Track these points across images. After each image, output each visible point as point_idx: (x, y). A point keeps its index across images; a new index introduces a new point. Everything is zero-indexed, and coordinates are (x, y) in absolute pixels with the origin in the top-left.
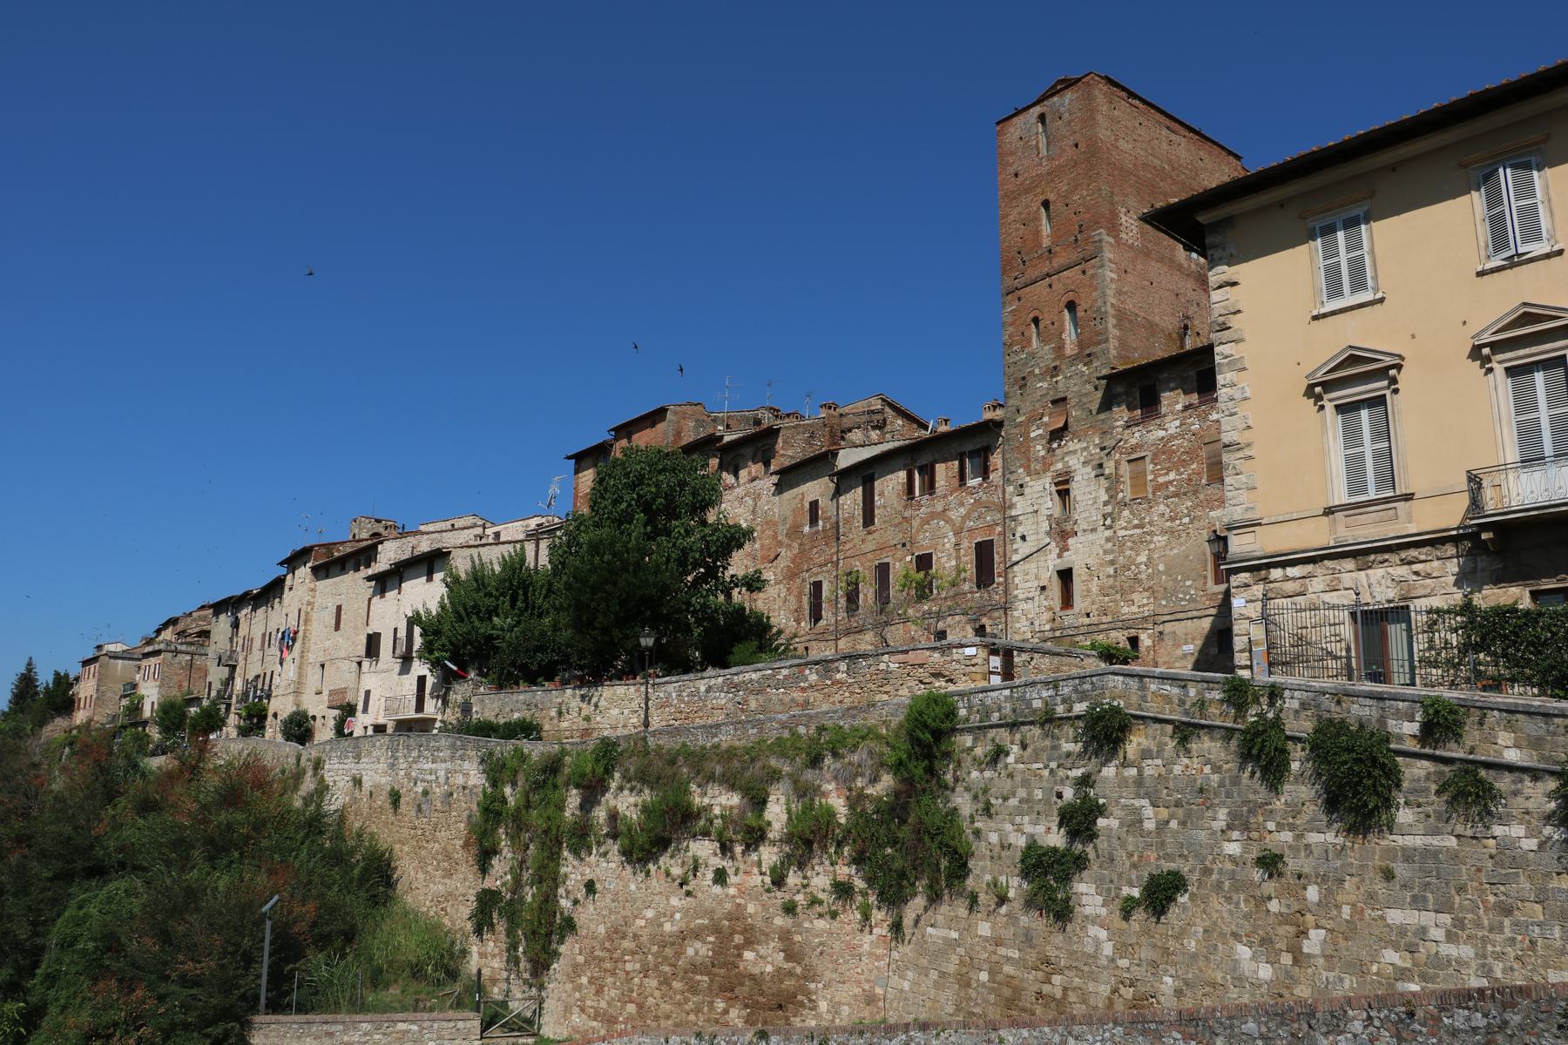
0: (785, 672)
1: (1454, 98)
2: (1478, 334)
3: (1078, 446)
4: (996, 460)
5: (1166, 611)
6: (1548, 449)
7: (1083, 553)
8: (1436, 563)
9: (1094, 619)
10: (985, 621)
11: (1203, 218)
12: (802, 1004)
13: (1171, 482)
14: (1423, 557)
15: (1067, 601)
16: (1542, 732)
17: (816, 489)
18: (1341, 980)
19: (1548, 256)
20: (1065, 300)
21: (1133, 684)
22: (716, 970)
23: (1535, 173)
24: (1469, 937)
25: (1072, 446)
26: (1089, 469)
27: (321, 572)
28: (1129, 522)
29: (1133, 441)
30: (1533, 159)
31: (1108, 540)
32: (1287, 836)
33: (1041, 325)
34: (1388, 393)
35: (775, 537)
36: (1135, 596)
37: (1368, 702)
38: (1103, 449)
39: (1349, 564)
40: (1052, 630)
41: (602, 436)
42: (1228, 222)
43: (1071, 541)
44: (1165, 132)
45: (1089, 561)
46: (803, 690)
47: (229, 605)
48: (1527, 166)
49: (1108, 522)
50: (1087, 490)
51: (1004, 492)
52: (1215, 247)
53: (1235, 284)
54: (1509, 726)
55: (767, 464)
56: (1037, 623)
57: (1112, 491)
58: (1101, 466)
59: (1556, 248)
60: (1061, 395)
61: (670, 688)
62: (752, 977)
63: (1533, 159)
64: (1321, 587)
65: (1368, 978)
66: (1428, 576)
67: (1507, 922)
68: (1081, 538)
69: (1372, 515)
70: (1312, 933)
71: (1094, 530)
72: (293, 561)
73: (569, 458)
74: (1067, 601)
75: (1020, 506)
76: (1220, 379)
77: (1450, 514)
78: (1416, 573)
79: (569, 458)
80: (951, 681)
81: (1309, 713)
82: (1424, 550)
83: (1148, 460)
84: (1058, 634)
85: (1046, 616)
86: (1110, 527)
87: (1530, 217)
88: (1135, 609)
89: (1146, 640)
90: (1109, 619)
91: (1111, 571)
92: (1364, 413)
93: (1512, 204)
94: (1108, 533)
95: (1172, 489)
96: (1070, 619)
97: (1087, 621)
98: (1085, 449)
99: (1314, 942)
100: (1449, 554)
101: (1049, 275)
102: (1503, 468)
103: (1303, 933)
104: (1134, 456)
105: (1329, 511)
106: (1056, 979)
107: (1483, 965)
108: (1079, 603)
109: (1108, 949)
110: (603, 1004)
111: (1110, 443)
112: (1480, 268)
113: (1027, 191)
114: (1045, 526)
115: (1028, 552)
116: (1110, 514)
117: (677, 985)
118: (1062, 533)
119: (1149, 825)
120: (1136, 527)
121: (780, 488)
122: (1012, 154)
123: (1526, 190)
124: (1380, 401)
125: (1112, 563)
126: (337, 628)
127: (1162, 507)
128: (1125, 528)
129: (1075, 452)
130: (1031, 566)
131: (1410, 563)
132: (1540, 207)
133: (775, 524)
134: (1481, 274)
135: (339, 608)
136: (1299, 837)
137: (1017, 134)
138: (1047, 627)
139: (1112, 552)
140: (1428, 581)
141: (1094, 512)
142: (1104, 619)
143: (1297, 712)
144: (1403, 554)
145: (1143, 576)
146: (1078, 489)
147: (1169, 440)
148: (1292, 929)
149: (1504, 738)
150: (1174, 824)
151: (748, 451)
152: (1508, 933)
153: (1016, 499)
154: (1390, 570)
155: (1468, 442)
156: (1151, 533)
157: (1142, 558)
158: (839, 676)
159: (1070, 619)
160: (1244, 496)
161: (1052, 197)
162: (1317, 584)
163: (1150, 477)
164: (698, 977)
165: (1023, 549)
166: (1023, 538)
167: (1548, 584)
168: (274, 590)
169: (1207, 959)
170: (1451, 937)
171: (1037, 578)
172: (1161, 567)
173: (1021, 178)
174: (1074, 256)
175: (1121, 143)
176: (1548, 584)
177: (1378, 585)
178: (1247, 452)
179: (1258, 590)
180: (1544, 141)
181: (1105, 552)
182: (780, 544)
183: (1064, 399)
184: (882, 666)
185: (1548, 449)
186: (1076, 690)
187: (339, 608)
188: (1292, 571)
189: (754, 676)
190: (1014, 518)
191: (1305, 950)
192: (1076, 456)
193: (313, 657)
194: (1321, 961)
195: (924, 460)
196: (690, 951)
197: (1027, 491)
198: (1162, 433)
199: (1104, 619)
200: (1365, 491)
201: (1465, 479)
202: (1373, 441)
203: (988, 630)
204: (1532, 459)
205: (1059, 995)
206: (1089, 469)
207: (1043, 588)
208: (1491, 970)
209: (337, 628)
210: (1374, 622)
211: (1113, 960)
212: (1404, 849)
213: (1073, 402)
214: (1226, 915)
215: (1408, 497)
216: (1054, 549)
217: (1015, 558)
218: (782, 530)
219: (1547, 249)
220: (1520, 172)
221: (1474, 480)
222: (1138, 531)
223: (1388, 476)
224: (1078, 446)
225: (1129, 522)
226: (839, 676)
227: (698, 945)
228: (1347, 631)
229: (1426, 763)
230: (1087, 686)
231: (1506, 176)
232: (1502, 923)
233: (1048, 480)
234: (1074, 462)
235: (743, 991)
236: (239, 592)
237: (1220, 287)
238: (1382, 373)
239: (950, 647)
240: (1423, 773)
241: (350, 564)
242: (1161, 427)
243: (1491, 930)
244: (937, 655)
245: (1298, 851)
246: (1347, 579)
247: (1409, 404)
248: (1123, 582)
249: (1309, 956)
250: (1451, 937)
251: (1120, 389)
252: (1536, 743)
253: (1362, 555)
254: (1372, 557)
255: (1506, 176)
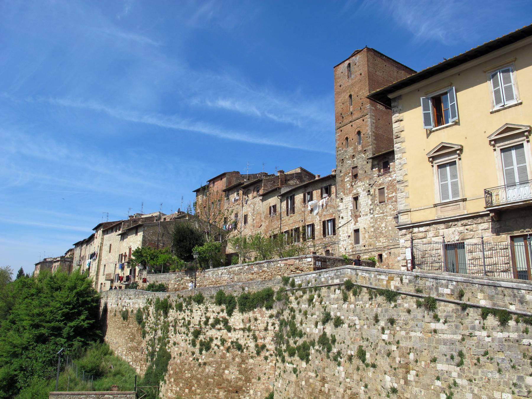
0: (247, 267)
1: (479, 46)
2: (490, 136)
3: (361, 184)
4: (333, 189)
5: (392, 244)
6: (517, 180)
7: (363, 223)
8: (474, 226)
9: (367, 248)
10: (329, 248)
11: (390, 96)
12: (244, 391)
13: (393, 197)
14: (469, 223)
15: (357, 241)
16: (493, 294)
17: (273, 200)
18: (421, 391)
19: (516, 105)
20: (357, 131)
21: (354, 272)
22: (215, 377)
23: (511, 73)
24: (466, 377)
25: (360, 184)
26: (365, 192)
27: (105, 232)
28: (379, 212)
29: (380, 182)
30: (510, 68)
31: (371, 218)
32: (403, 333)
33: (349, 140)
34: (457, 160)
35: (260, 219)
36: (381, 239)
37: (432, 280)
38: (370, 185)
39: (442, 226)
40: (353, 252)
41: (205, 184)
42: (399, 97)
43: (359, 219)
44: (395, 69)
45: (365, 226)
46: (252, 274)
47: (79, 244)
48: (508, 71)
49: (372, 212)
50: (364, 201)
51: (336, 201)
52: (394, 107)
53: (402, 120)
54: (482, 291)
55: (258, 191)
56: (347, 249)
57: (373, 200)
58: (369, 191)
59: (519, 102)
60: (355, 165)
61: (210, 273)
62: (227, 380)
63: (510, 68)
64: (431, 235)
65: (430, 391)
66: (471, 230)
67: (480, 371)
68: (362, 218)
69: (451, 207)
70: (411, 372)
71: (367, 215)
72: (97, 229)
73: (194, 191)
74: (357, 241)
75: (342, 206)
76: (396, 156)
77: (479, 206)
78: (467, 229)
79: (194, 191)
80: (302, 271)
81: (411, 284)
82: (470, 220)
83: (385, 188)
84: (354, 253)
85: (350, 247)
86: (372, 214)
87: (509, 90)
88: (381, 244)
89: (385, 256)
90: (372, 248)
91: (372, 230)
92: (448, 168)
93: (502, 86)
94: (372, 216)
95: (394, 199)
96: (359, 247)
97: (364, 248)
98: (364, 185)
99: (411, 377)
100: (479, 222)
101: (351, 122)
102: (497, 188)
103: (408, 372)
104: (381, 187)
105: (435, 206)
106: (326, 385)
107: (471, 388)
108: (361, 242)
109: (343, 375)
110: (178, 389)
111: (372, 183)
112: (491, 111)
113: (344, 91)
114: (350, 213)
115: (344, 223)
116: (372, 209)
117: (202, 382)
118: (356, 216)
119: (358, 327)
120: (381, 213)
121: (262, 200)
122: (339, 78)
123: (507, 80)
124: (454, 163)
125: (373, 227)
126: (110, 252)
127: (390, 206)
128: (377, 214)
129: (360, 186)
130: (345, 228)
131: (465, 225)
132: (513, 86)
133: (261, 214)
134: (491, 113)
135: (111, 245)
136: (407, 333)
137: (341, 71)
138: (351, 251)
139: (373, 223)
140: (472, 232)
141: (367, 208)
142: (370, 248)
143: (407, 284)
144: (462, 222)
145: (384, 232)
146: (361, 200)
147: (393, 181)
148: (404, 370)
149: (480, 296)
150: (365, 327)
151: (252, 188)
152: (480, 375)
153: (340, 204)
154: (457, 228)
155: (485, 177)
156: (387, 216)
157: (383, 225)
158: (264, 269)
159: (359, 247)
160: (403, 201)
161: (352, 93)
162: (430, 234)
163: (386, 195)
164: (210, 380)
165: (342, 222)
166: (342, 218)
167: (517, 233)
168: (92, 238)
169: (375, 380)
170: (459, 376)
171: (347, 232)
172: (390, 228)
173: (342, 87)
174: (360, 115)
175: (378, 73)
176: (517, 233)
177: (452, 234)
178: (406, 184)
179: (409, 236)
180: (515, 61)
181: (371, 223)
182: (262, 221)
183: (356, 167)
184: (279, 265)
185: (517, 180)
186: (335, 275)
187: (111, 245)
188: (421, 229)
189: (237, 269)
190: (339, 211)
191: (409, 379)
192: (361, 188)
193: (103, 263)
194: (414, 383)
195: (309, 190)
196: (207, 370)
197: (344, 201)
198: (390, 179)
199: (370, 248)
200: (448, 198)
201: (483, 193)
202: (451, 179)
203: (330, 252)
204: (511, 184)
205: (327, 392)
206: (365, 192)
207: (349, 236)
208: (473, 391)
209: (110, 252)
210: (454, 248)
211: (345, 379)
212: (444, 340)
213: (360, 168)
214: (382, 363)
215: (464, 200)
216: (353, 222)
217: (340, 225)
218: (263, 216)
219: (516, 103)
220: (505, 74)
221: (488, 193)
222: (382, 215)
223: (455, 193)
224: (361, 184)
225: (379, 212)
226: (264, 269)
227: (210, 367)
228: (441, 252)
229: (452, 305)
230: (339, 273)
231: (500, 76)
232: (478, 371)
233: (351, 197)
234: (360, 190)
235: (224, 385)
236: (82, 240)
237: (396, 122)
238: (454, 152)
239: (302, 258)
240: (451, 309)
241: (114, 229)
242: (390, 176)
243: (474, 374)
244: (297, 261)
245: (407, 339)
246: (441, 232)
247: (464, 163)
248: (377, 234)
249: (410, 381)
250: (459, 376)
251: (376, 163)
252: (491, 298)
253: (447, 222)
254: (451, 223)
255: (500, 76)
